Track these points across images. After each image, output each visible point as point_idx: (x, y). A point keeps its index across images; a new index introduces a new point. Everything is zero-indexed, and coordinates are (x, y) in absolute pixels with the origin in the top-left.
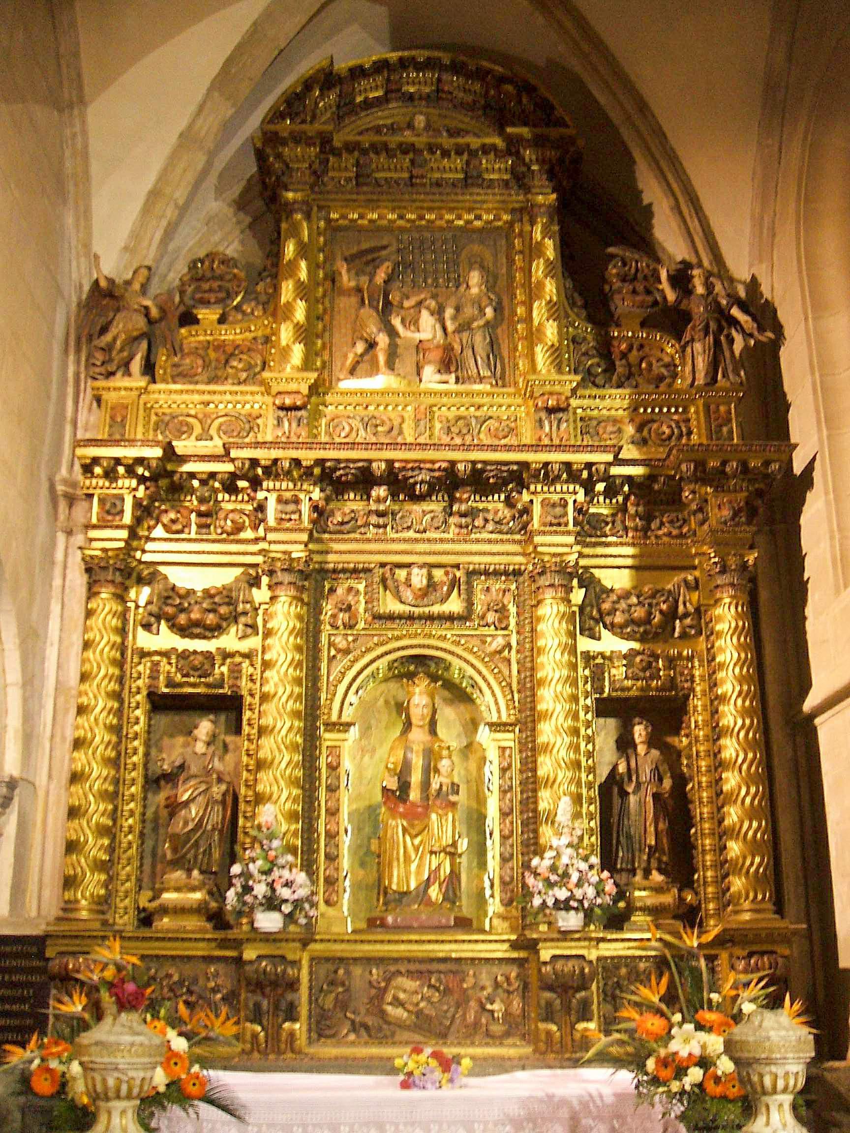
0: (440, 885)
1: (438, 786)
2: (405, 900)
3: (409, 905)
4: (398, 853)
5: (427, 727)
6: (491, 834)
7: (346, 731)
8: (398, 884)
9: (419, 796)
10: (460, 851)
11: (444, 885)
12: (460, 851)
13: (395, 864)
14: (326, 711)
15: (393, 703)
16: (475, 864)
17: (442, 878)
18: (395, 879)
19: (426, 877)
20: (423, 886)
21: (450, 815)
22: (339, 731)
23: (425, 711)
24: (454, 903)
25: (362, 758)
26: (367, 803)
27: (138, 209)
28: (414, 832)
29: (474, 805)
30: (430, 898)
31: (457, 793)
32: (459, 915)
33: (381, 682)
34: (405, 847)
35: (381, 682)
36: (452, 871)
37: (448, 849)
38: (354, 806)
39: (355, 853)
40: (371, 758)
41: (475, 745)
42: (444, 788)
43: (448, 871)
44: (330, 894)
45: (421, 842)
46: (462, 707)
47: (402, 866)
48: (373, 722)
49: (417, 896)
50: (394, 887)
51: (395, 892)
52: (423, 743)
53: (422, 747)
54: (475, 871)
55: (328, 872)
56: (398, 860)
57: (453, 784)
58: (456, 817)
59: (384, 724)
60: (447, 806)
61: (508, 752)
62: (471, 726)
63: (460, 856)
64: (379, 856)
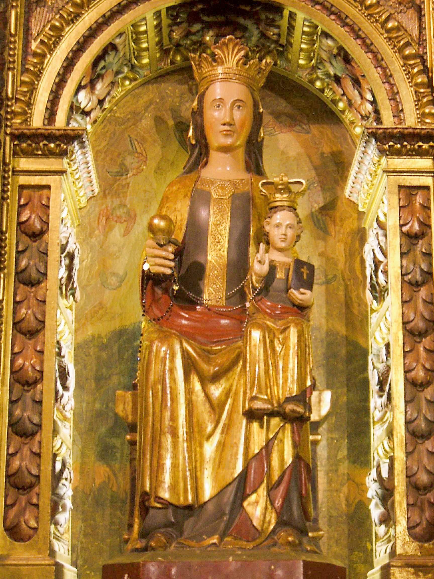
0: (270, 490)
1: (265, 268)
2: (189, 524)
3: (198, 537)
4: (174, 418)
5: (241, 154)
6: (382, 383)
7: (63, 154)
8: (173, 488)
9: (222, 294)
10: (314, 417)
11: (281, 490)
12: (314, 417)
13: (168, 440)
14: (17, 108)
15: (171, 123)
16: (344, 452)
17: (276, 475)
18: (167, 478)
19: (239, 468)
20: (232, 490)
21: (293, 333)
22: (50, 154)
23: (238, 115)
24: (303, 532)
25: (106, 234)
26: (116, 325)
27: (139, 297)
28: (212, 370)
29: (342, 330)
30: (249, 519)
31: (309, 286)
32: (315, 559)
33: (148, 82)
34: (190, 403)
35: (148, 82)
36: (297, 458)
37: (289, 407)
38: (90, 331)
39: (91, 429)
40: (127, 232)
41: (342, 207)
42: (280, 275)
43: (289, 459)
44: (22, 512)
45: (227, 394)
46: (315, 129)
47: (183, 445)
48: (130, 161)
49: (220, 513)
50: (166, 495)
51: (167, 505)
52: (233, 183)
53: (229, 191)
54: (344, 467)
55: (16, 463)
56: (175, 435)
57: (299, 263)
58: (310, 338)
59: (152, 164)
60: (285, 312)
61: (419, 199)
62: (332, 167)
63: (316, 426)
64: (133, 428)
